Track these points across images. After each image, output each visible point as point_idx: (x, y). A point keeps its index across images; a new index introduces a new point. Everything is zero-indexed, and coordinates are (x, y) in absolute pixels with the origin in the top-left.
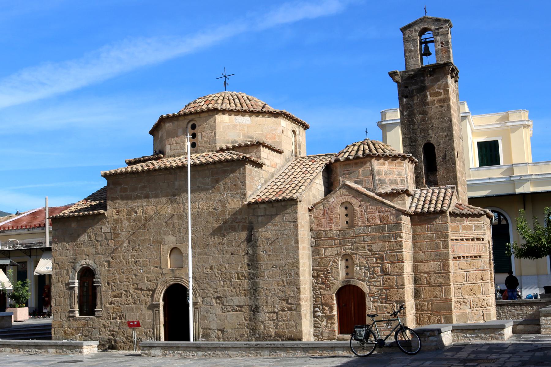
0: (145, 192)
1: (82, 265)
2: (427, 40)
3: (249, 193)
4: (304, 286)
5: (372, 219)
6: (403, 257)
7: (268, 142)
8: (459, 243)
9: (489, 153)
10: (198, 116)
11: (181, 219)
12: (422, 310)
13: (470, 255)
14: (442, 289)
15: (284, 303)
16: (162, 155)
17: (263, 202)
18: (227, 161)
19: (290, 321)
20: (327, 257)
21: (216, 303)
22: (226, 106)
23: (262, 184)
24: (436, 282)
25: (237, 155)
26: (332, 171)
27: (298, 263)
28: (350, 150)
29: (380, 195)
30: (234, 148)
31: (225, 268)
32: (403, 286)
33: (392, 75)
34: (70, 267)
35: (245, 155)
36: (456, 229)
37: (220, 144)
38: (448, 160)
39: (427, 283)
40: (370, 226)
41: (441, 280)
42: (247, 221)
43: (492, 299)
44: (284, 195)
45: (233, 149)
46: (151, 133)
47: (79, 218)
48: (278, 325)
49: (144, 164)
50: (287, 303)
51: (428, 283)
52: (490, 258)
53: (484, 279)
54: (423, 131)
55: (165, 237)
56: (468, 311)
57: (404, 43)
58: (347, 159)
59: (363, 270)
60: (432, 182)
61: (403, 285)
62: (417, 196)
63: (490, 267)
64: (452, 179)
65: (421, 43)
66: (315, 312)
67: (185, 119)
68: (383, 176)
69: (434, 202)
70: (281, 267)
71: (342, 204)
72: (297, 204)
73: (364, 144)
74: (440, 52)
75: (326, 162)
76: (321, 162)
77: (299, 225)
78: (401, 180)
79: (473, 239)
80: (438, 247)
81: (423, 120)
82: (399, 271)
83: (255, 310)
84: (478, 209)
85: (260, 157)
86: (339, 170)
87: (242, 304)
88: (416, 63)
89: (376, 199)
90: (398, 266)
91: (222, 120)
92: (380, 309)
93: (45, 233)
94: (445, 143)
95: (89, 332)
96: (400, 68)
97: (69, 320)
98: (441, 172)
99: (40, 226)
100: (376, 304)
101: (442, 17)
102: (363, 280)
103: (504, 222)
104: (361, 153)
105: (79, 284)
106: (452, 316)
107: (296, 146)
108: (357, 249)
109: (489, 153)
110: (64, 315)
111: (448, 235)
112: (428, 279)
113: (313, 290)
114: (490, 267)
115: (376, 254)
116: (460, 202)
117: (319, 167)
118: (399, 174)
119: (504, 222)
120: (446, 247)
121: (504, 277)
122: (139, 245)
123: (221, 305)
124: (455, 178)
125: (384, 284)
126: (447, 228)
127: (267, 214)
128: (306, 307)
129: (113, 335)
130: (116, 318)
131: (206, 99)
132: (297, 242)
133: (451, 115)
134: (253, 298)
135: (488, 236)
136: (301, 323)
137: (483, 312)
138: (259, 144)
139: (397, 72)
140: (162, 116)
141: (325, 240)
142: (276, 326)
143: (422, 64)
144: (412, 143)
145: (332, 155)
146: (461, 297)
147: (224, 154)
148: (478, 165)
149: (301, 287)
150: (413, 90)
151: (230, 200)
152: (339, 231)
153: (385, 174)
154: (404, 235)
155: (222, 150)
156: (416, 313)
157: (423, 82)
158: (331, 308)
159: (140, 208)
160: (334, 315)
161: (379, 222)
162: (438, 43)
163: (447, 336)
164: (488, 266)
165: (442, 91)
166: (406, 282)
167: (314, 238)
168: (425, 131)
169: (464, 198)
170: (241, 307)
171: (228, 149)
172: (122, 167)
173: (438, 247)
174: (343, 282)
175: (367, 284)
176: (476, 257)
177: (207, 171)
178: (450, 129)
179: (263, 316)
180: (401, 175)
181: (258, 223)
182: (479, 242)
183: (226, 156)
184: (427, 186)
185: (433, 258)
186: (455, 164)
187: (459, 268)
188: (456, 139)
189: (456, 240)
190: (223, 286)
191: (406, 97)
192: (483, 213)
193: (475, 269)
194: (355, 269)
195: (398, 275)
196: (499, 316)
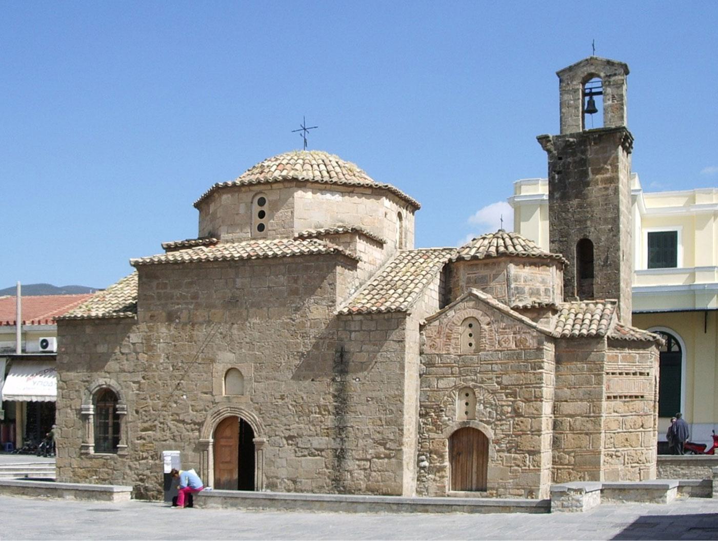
0: (192, 290)
1: (99, 386)
2: (593, 91)
3: (339, 299)
4: (408, 427)
5: (505, 342)
6: (542, 394)
7: (367, 229)
8: (617, 378)
9: (663, 249)
10: (269, 187)
11: (242, 330)
12: (561, 464)
13: (630, 394)
14: (590, 437)
15: (382, 449)
16: (215, 239)
17: (359, 313)
18: (311, 253)
19: (387, 471)
20: (439, 390)
21: (288, 444)
22: (308, 175)
23: (357, 287)
24: (583, 428)
25: (324, 246)
26: (451, 272)
27: (402, 396)
28: (478, 245)
29: (516, 309)
30: (319, 236)
31: (302, 398)
32: (539, 432)
33: (543, 140)
34: (84, 388)
35: (336, 247)
36: (614, 359)
37: (300, 227)
38: (610, 265)
39: (570, 430)
40: (501, 351)
41: (589, 426)
42: (335, 337)
43: (653, 453)
44: (388, 304)
45: (316, 237)
46: (197, 206)
47: (97, 322)
48: (370, 475)
49: (190, 251)
50: (385, 448)
51: (572, 429)
52: (655, 399)
53: (644, 426)
54: (579, 221)
55: (219, 352)
56: (620, 467)
57: (561, 94)
58: (475, 258)
59: (488, 410)
60: (587, 294)
61: (539, 430)
62: (565, 312)
63: (654, 411)
64: (613, 291)
65: (584, 95)
66: (420, 461)
67: (250, 191)
68: (521, 284)
69: (587, 322)
70: (378, 401)
71: (465, 319)
72: (405, 318)
73: (498, 238)
74: (609, 109)
75: (446, 260)
76: (437, 260)
77: (407, 346)
78: (546, 289)
79: (634, 374)
80: (589, 382)
81: (580, 206)
82: (535, 412)
83: (340, 455)
84: (641, 333)
85: (355, 249)
86: (462, 275)
87: (323, 447)
88: (575, 127)
89: (511, 316)
90: (535, 406)
91: (303, 198)
92: (506, 460)
93: (15, 334)
94: (607, 240)
95: (108, 474)
96: (553, 131)
97: (82, 459)
98: (598, 279)
99: (8, 324)
100: (502, 454)
101: (616, 59)
102: (488, 423)
103: (675, 348)
104: (493, 249)
105: (95, 410)
106: (599, 473)
107: (401, 233)
108: (483, 382)
109: (663, 249)
110: (74, 451)
111: (603, 367)
112: (572, 424)
113: (419, 433)
114: (654, 411)
115: (507, 388)
116: (622, 324)
117: (435, 266)
118: (543, 282)
119: (675, 348)
120: (600, 383)
121: (667, 423)
122: (182, 362)
123: (294, 447)
124: (618, 289)
125: (514, 428)
126: (603, 357)
127: (363, 329)
128: (409, 452)
129: (142, 480)
130: (146, 458)
131: (279, 162)
132: (402, 368)
133: (619, 202)
134: (338, 440)
135: (655, 371)
136: (402, 474)
137: (640, 470)
138: (357, 232)
139: (548, 137)
140: (217, 185)
141: (440, 367)
142: (368, 477)
143: (583, 127)
144: (562, 237)
145: (451, 250)
146: (613, 449)
147: (305, 243)
148: (645, 267)
149: (405, 428)
150: (570, 163)
151: (312, 308)
152: (460, 356)
153: (525, 281)
154: (545, 365)
155: (302, 237)
156: (553, 468)
157: (584, 152)
158: (441, 456)
159: (185, 312)
160: (445, 467)
161: (514, 347)
162: (608, 97)
163: (595, 496)
164: (652, 410)
165: (609, 167)
166: (544, 427)
167: (424, 364)
168: (582, 222)
169: (627, 317)
170: (322, 450)
171: (310, 236)
172: (161, 256)
173: (589, 382)
174: (460, 423)
175: (492, 428)
176: (636, 397)
177: (282, 267)
178: (616, 220)
179: (350, 464)
180: (546, 283)
181: (351, 340)
182: (642, 377)
183: (306, 247)
184: (578, 298)
185: (581, 396)
186: (618, 270)
187: (614, 412)
188: (622, 236)
189: (613, 374)
190: (297, 423)
191: (558, 173)
192: (651, 339)
193: (634, 413)
194: (477, 407)
195: (535, 418)
196: (659, 475)
